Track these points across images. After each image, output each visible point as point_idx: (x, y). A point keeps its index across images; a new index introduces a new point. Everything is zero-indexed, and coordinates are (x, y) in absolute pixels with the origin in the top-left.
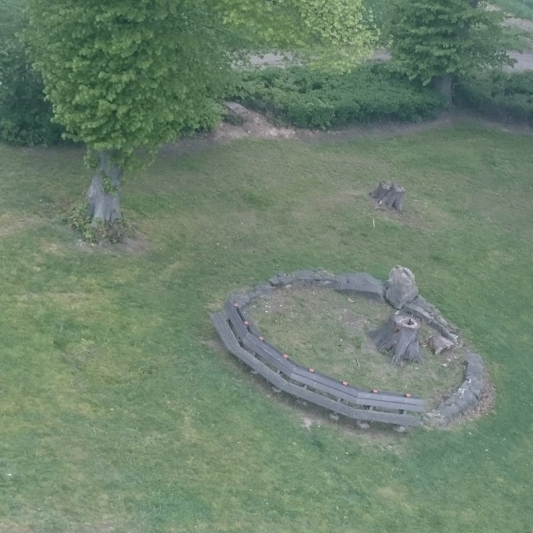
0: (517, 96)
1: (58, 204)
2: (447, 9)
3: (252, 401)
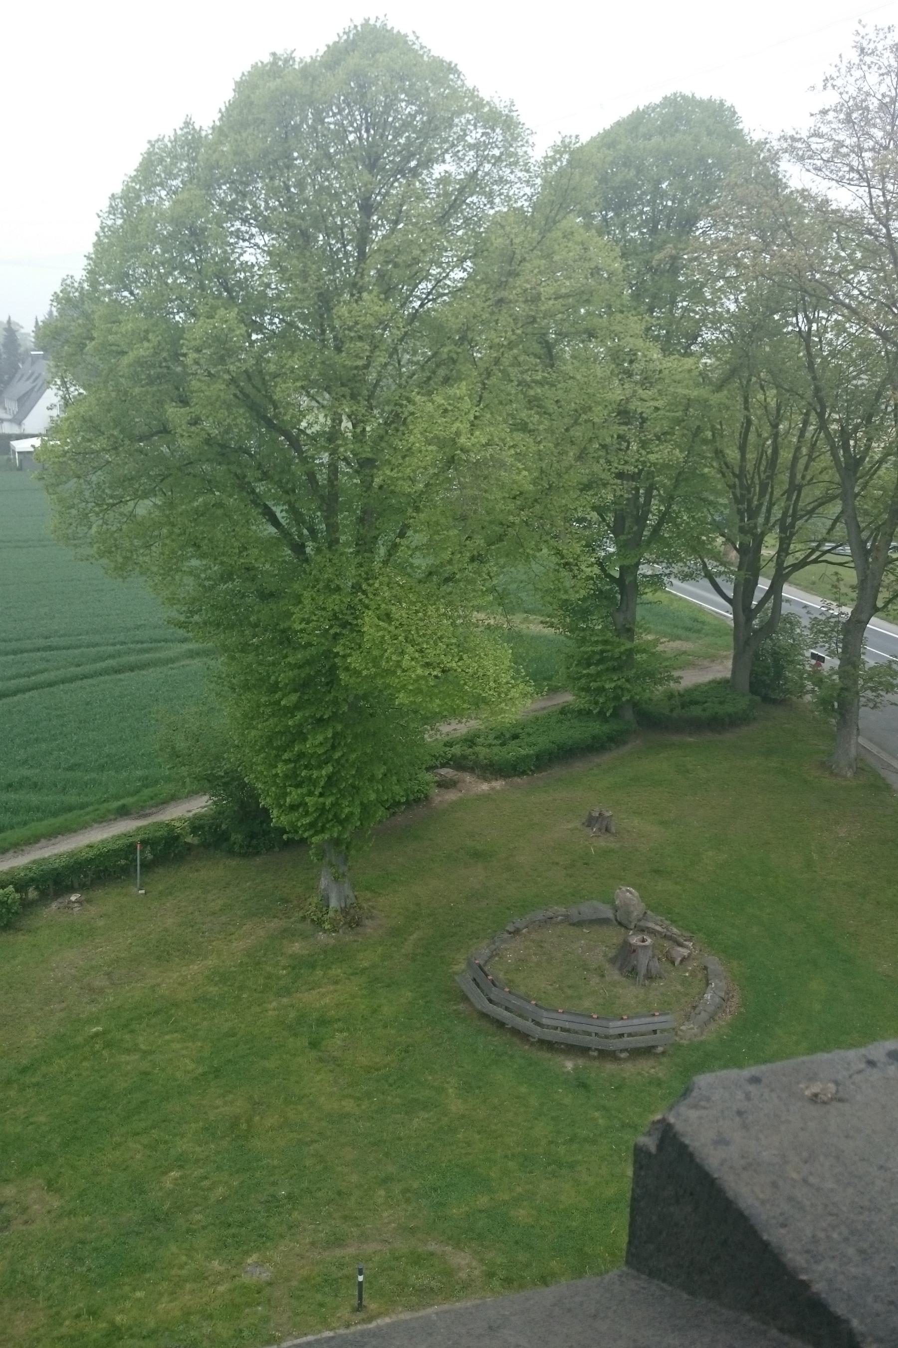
0: (693, 707)
1: (295, 902)
2: (609, 647)
3: (512, 1057)
